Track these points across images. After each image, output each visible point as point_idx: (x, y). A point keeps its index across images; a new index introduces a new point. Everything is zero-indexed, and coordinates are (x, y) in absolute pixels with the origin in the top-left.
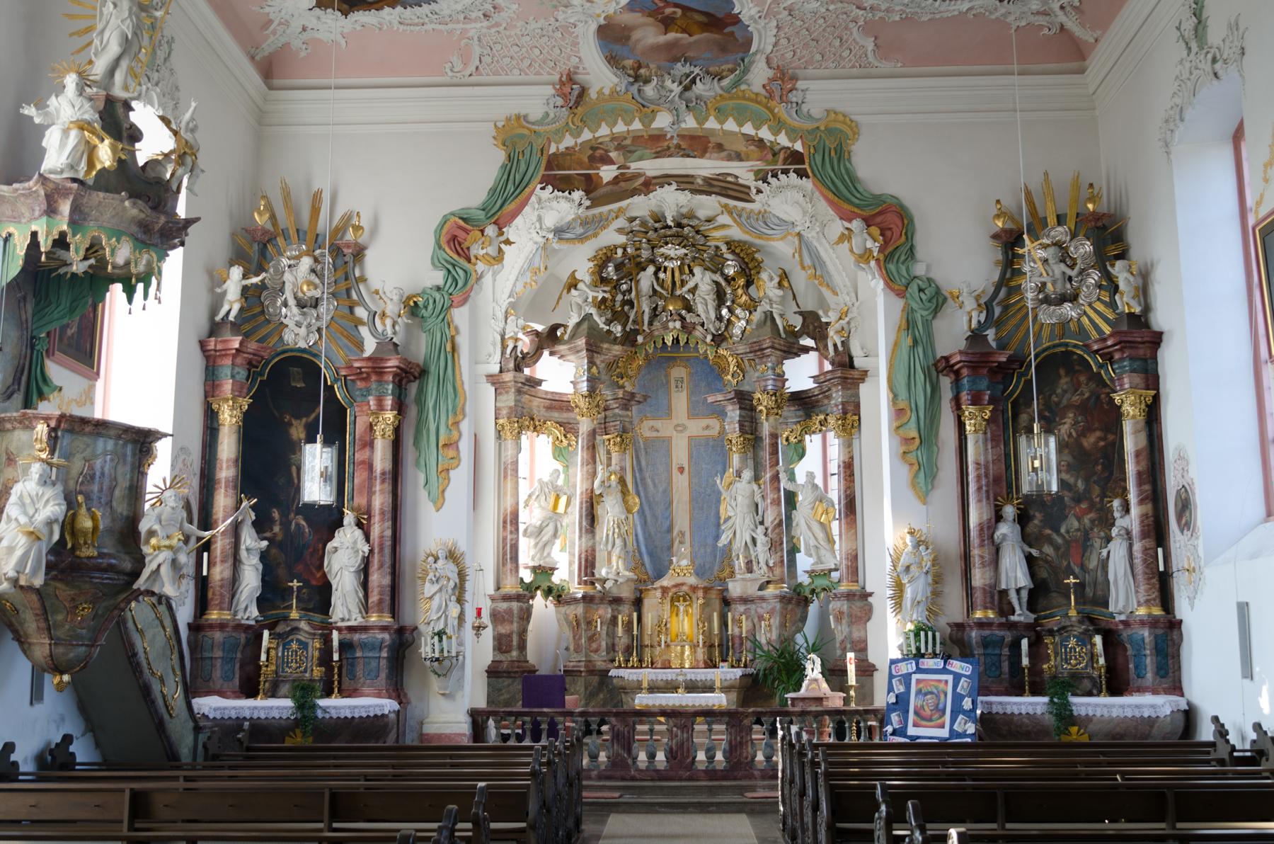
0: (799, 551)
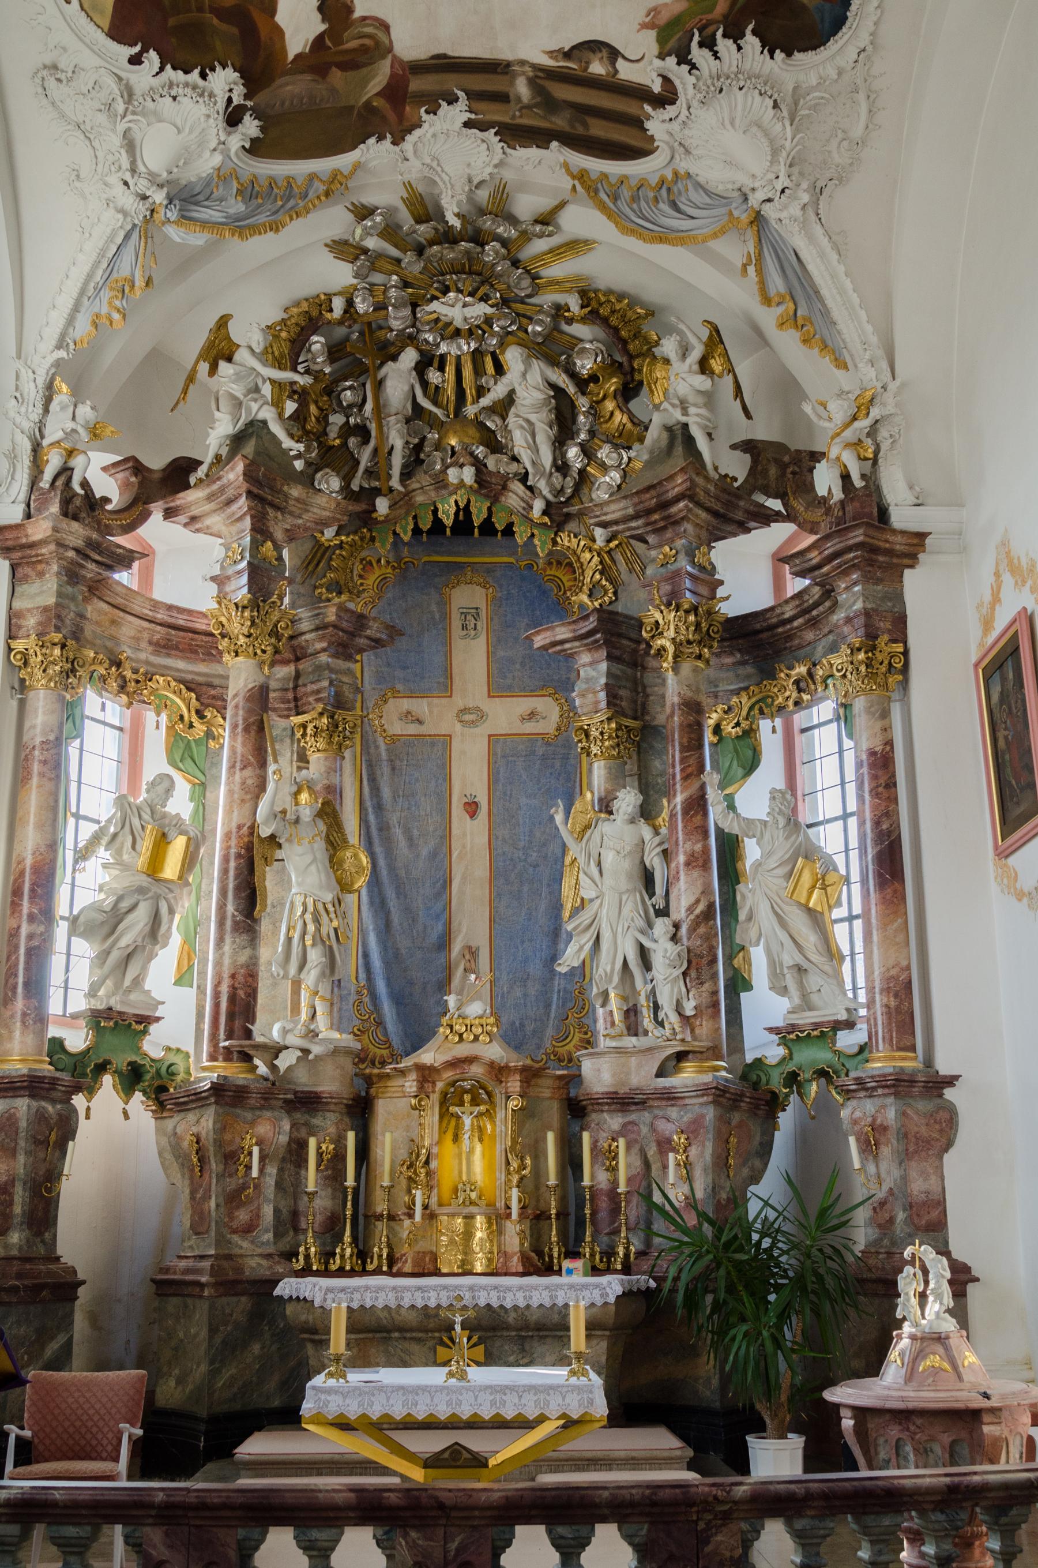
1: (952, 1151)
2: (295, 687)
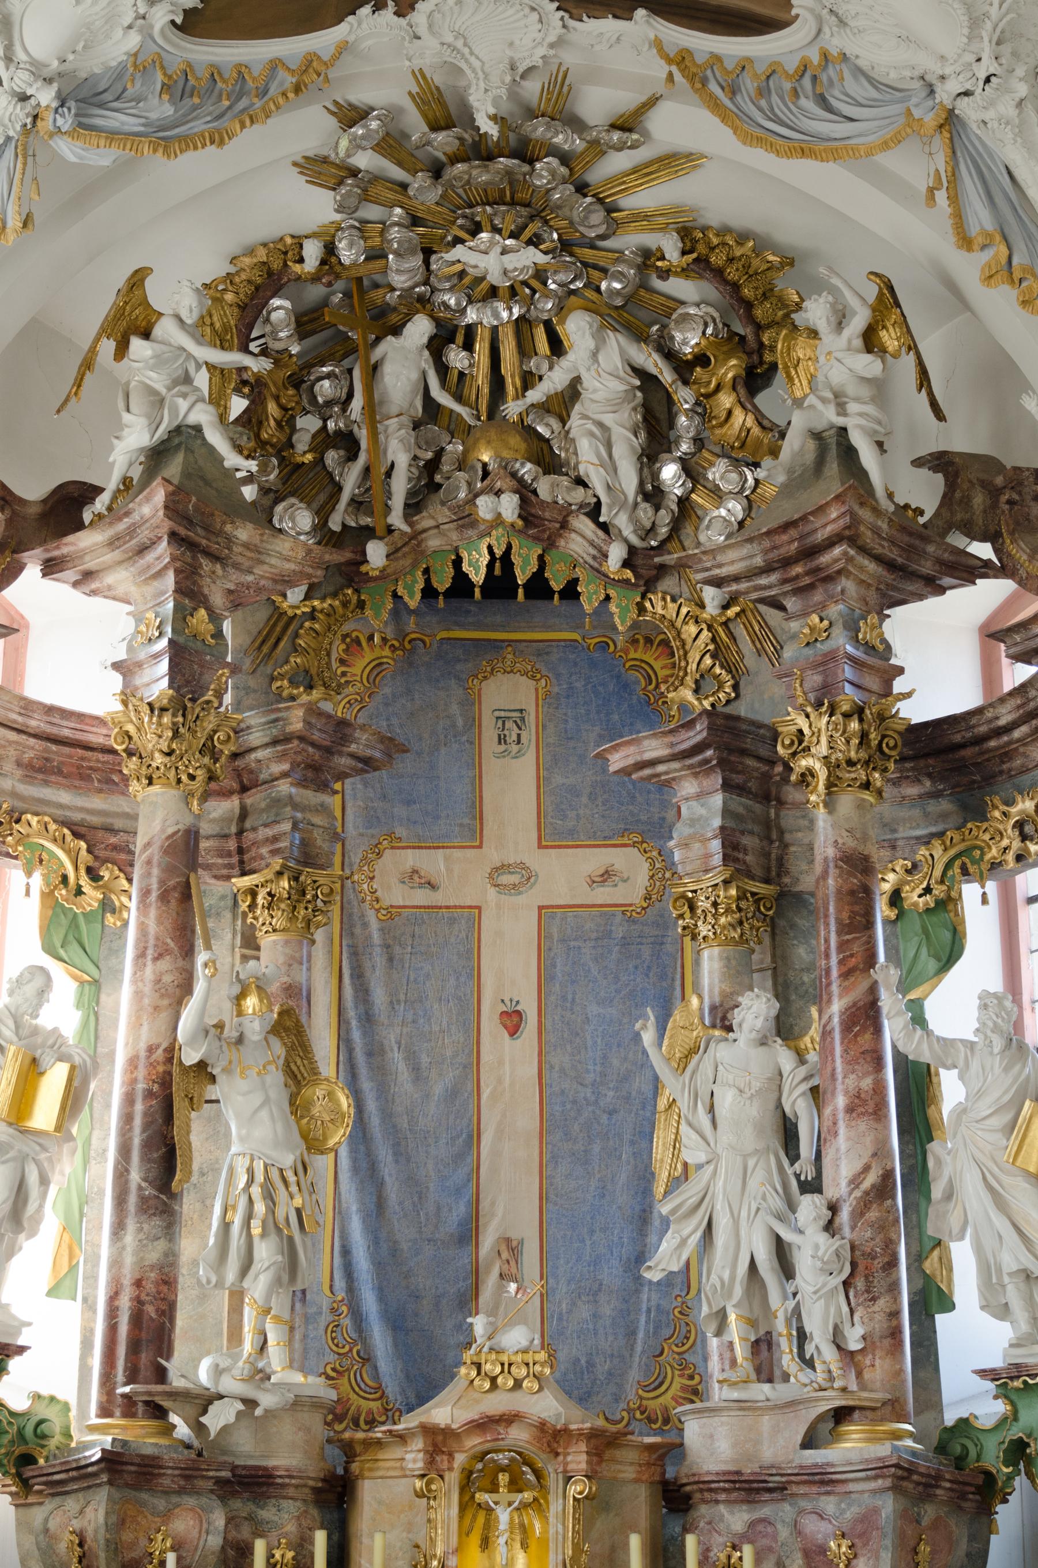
0: (948, 1305)
2: (240, 833)
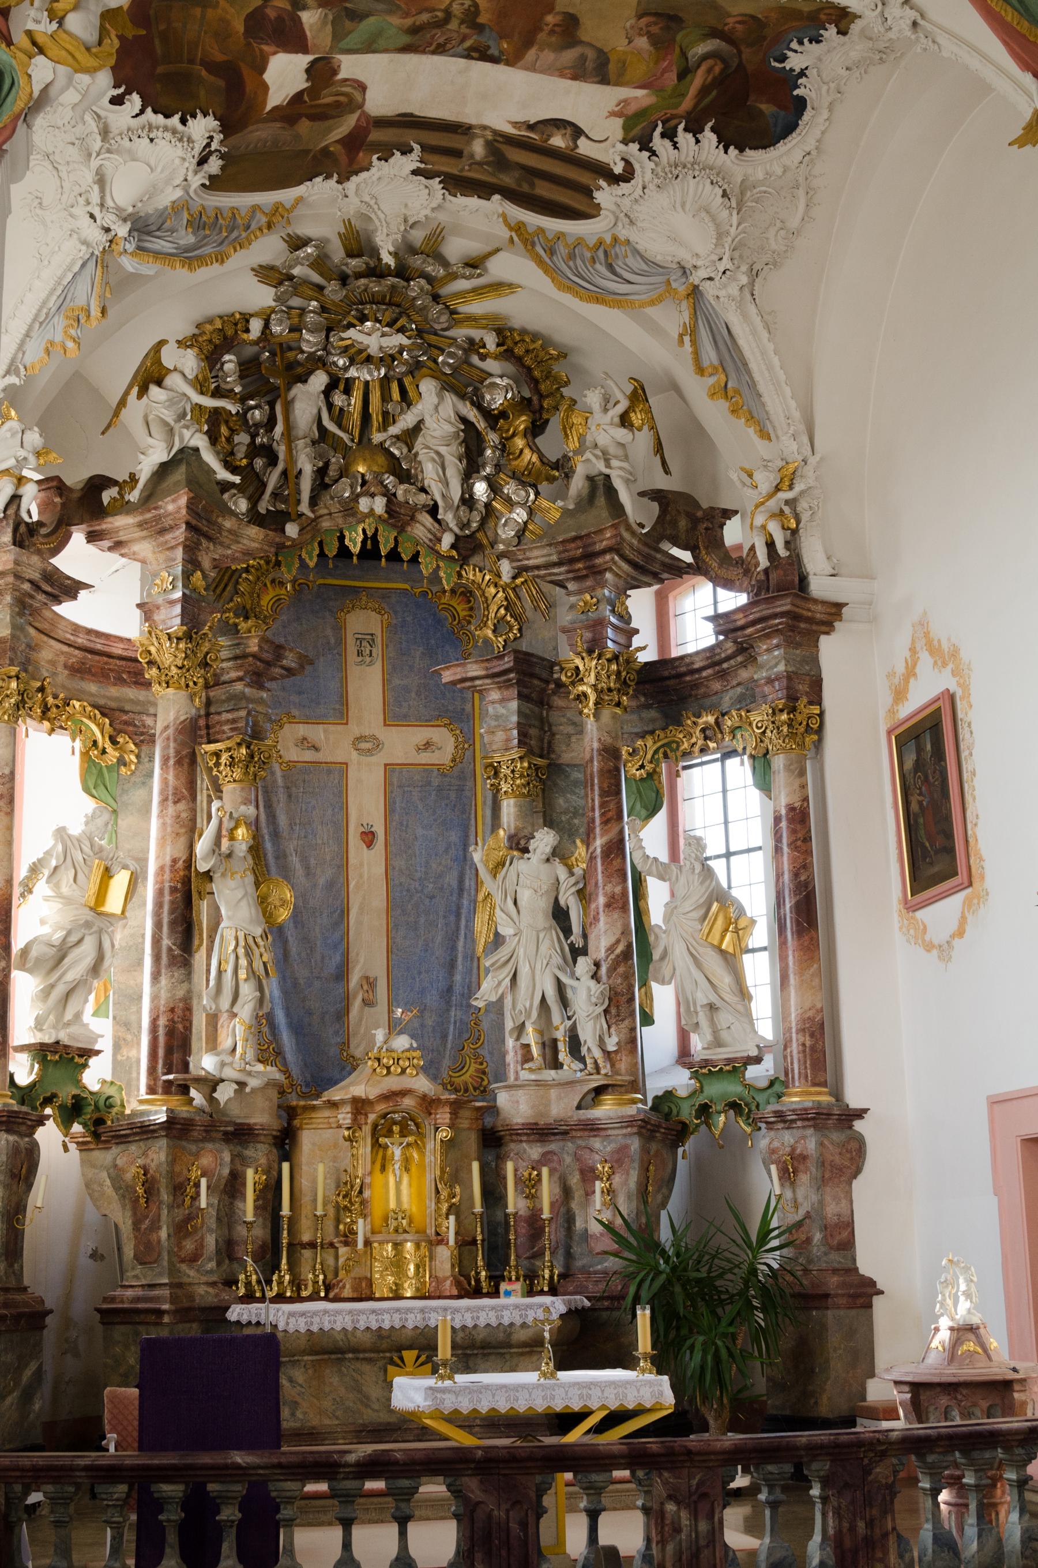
1: (860, 1177)
2: (208, 715)
